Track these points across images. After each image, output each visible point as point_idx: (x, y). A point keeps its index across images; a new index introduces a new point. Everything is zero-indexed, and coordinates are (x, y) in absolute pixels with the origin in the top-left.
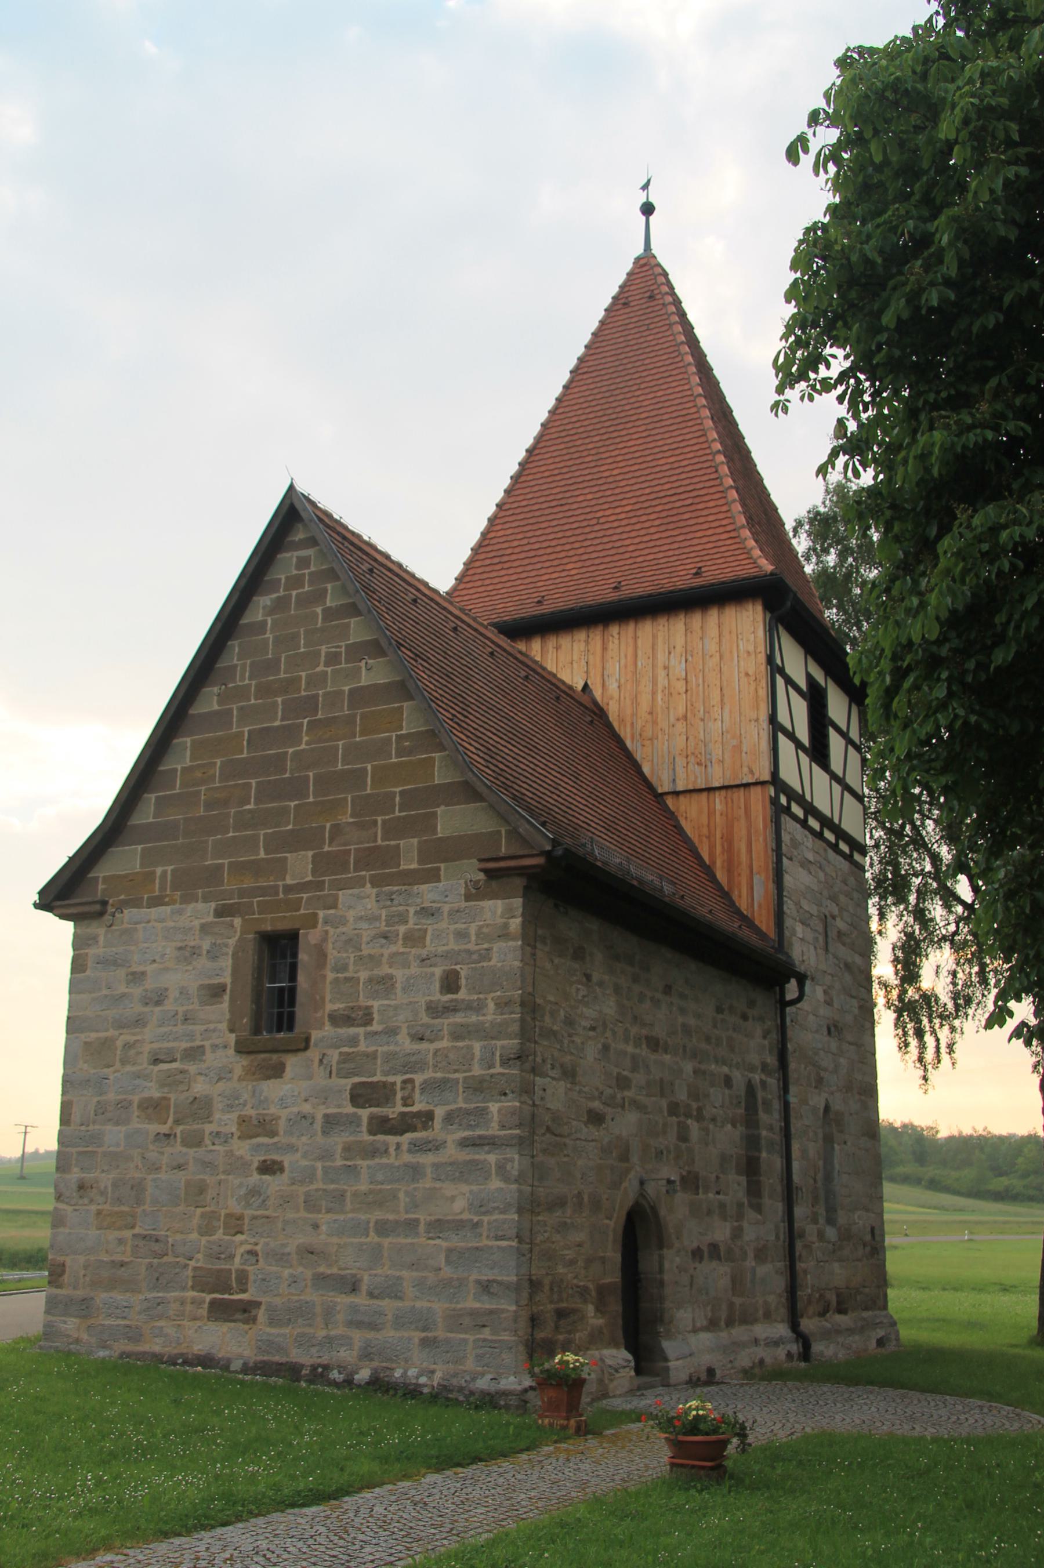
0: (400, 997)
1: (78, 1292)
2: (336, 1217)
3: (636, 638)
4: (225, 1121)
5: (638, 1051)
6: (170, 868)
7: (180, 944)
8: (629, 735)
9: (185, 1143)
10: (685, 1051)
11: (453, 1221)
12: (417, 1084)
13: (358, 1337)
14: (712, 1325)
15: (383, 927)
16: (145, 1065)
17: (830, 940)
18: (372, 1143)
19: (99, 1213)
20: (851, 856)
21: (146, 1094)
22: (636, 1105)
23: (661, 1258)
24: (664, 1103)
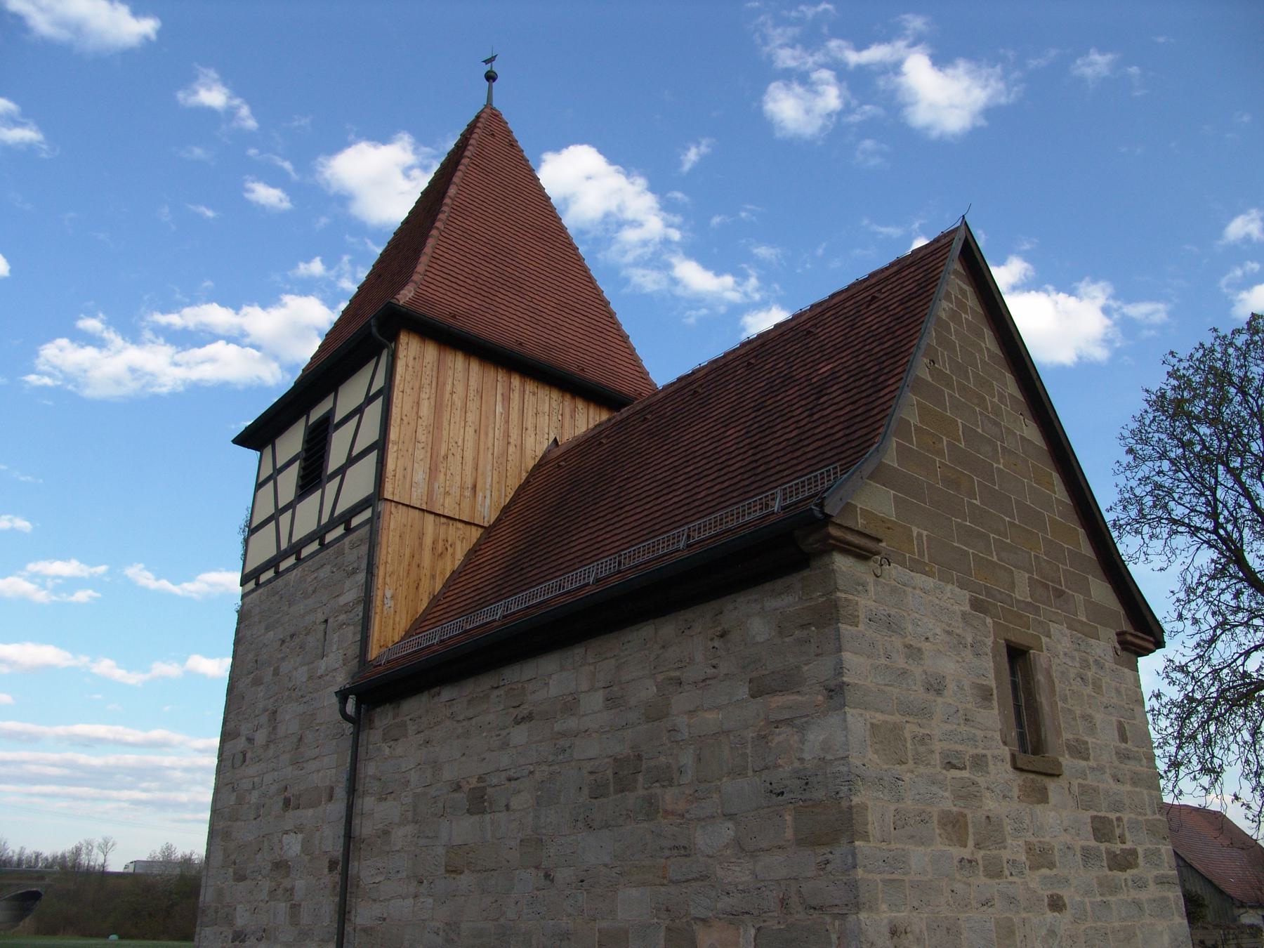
4: (1014, 849)
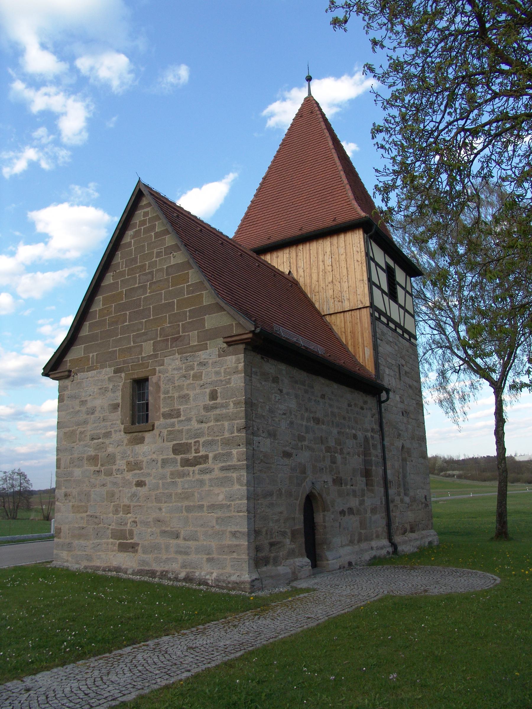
3: (310, 250)
4: (121, 464)
5: (309, 424)
6: (95, 354)
7: (100, 387)
9: (105, 475)
10: (333, 424)
11: (219, 505)
12: (201, 443)
14: (351, 542)
15: (183, 372)
16: (88, 441)
17: (401, 375)
18: (183, 471)
19: (73, 506)
21: (90, 454)
23: (324, 516)
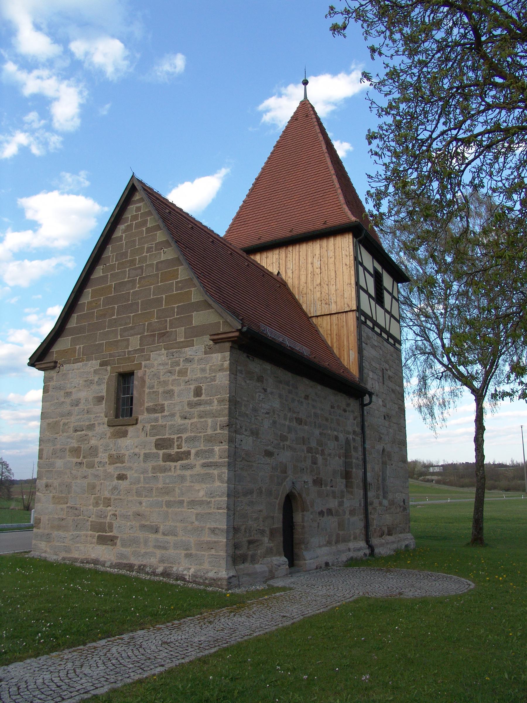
0: (176, 399)
1: (46, 531)
2: (149, 499)
3: (299, 252)
4: (103, 457)
8: (297, 293)
10: (315, 425)
13: (159, 552)
14: (329, 543)
15: (169, 367)
17: (385, 379)
20: (395, 345)
21: (72, 445)
22: (290, 448)
24: (305, 448)
